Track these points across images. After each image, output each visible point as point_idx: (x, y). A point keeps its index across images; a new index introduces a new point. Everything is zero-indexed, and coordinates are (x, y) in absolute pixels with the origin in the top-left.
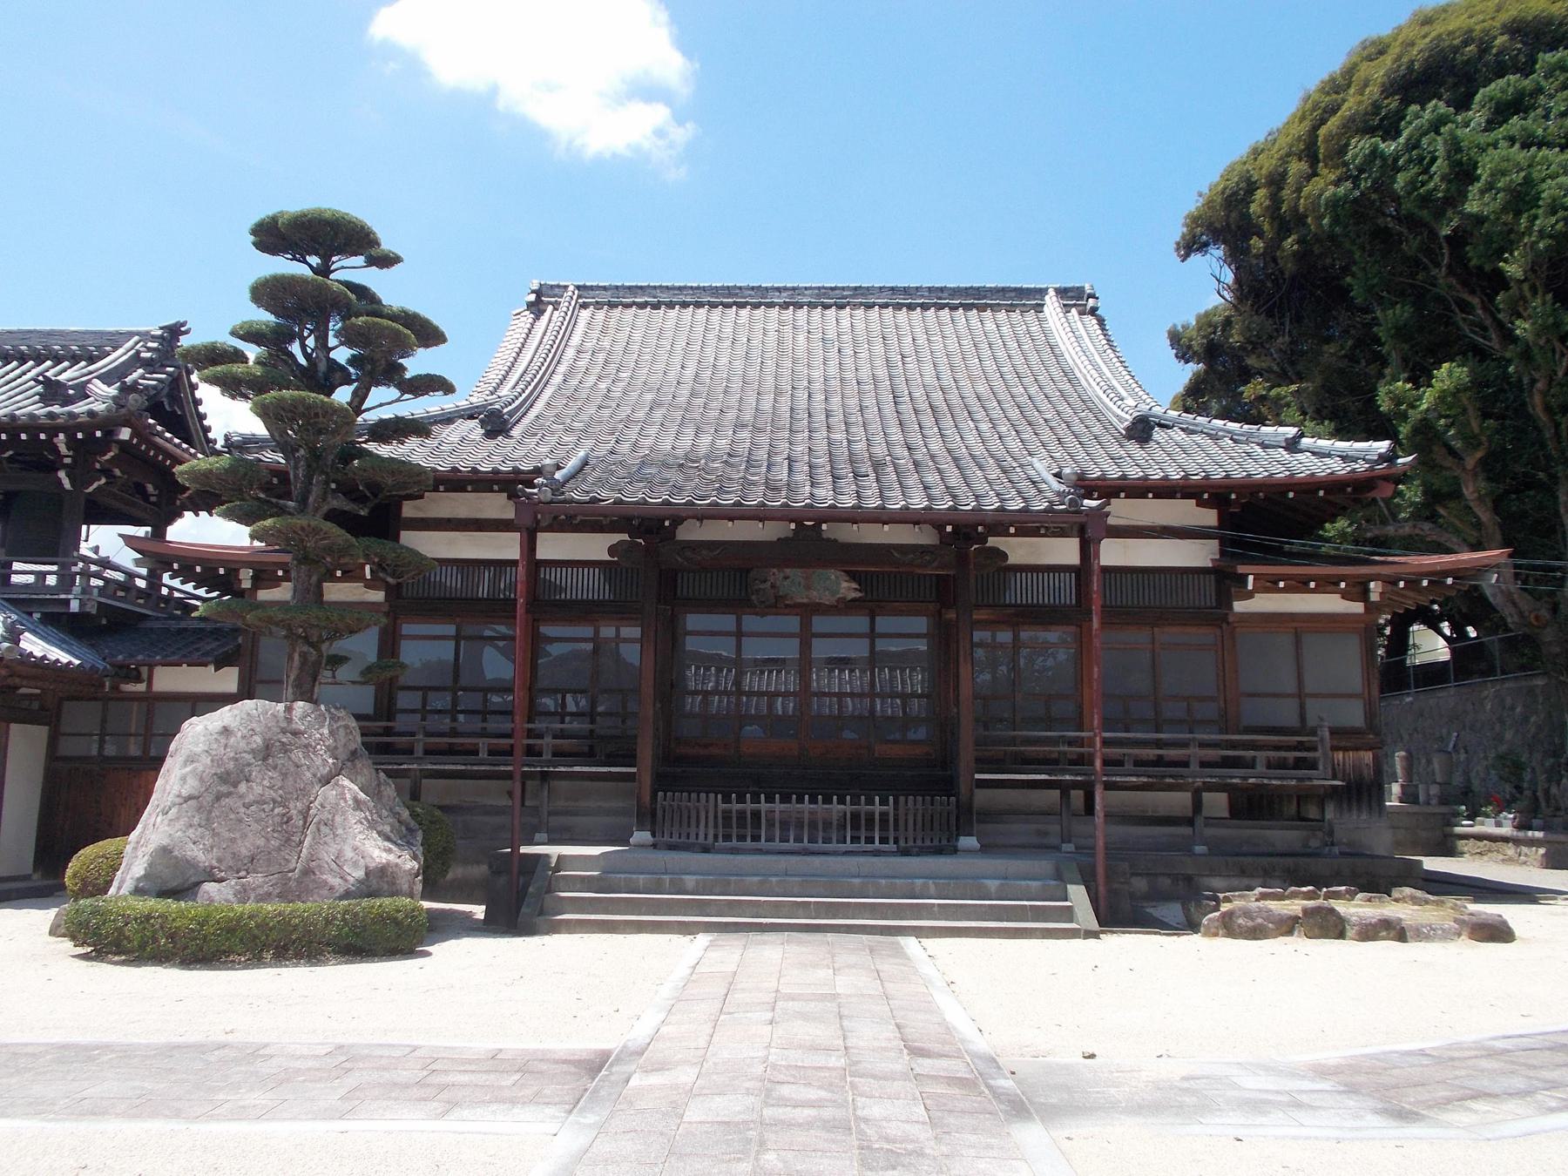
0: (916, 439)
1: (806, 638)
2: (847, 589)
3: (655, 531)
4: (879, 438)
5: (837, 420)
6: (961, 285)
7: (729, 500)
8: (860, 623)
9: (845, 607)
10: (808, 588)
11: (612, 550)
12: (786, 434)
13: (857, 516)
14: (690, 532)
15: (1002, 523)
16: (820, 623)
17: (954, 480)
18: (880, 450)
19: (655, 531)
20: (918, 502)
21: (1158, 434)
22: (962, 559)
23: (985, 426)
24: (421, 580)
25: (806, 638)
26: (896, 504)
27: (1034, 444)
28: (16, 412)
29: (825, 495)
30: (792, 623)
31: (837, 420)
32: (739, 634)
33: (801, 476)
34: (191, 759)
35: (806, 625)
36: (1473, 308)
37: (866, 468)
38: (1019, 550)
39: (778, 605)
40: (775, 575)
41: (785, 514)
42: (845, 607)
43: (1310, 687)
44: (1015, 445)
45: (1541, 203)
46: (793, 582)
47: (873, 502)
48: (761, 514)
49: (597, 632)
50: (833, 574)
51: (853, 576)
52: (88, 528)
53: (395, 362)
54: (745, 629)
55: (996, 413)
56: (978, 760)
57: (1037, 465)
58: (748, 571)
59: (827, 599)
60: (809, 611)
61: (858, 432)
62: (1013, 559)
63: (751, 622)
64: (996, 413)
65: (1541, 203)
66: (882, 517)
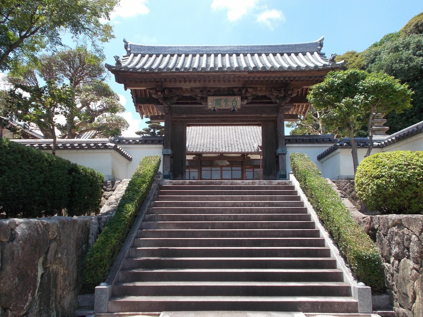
0: (238, 140)
2: (228, 163)
4: (232, 140)
5: (226, 136)
7: (211, 151)
8: (229, 168)
9: (227, 166)
10: (222, 163)
11: (193, 158)
12: (218, 139)
13: (228, 153)
14: (204, 155)
15: (248, 153)
16: (224, 168)
17: (243, 147)
18: (232, 142)
20: (237, 151)
22: (244, 158)
23: (249, 137)
24: (84, 138)
26: (233, 151)
27: (256, 141)
29: (224, 150)
30: (219, 169)
31: (226, 136)
32: (211, 170)
33: (220, 147)
34: (110, 204)
35: (221, 169)
37: (230, 145)
38: (253, 157)
39: (217, 166)
40: (217, 161)
41: (219, 153)
42: (227, 166)
43: (231, 171)
44: (253, 140)
46: (219, 162)
47: (230, 151)
48: (215, 153)
49: (189, 171)
50: (225, 161)
51: (228, 161)
52: (197, 172)
54: (212, 169)
55: (251, 135)
57: (255, 144)
58: (212, 161)
59: (225, 165)
60: (222, 167)
61: (229, 138)
62: (251, 158)
63: (213, 169)
64: (251, 135)
66: (232, 153)
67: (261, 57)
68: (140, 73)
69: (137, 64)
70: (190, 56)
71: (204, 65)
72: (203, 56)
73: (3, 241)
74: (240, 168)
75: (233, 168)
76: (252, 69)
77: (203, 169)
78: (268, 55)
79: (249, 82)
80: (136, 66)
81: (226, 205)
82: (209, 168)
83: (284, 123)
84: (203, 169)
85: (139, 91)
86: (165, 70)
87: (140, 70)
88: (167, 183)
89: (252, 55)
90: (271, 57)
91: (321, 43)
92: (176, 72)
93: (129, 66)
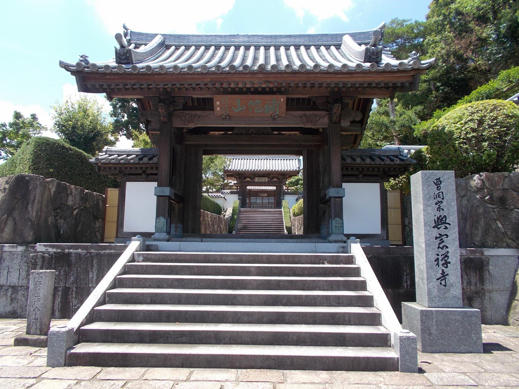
1: (262, 199)
2: (266, 195)
3: (490, 16)
6: (249, 34)
8: (267, 198)
16: (264, 198)
19: (490, 16)
21: (12, 341)
25: (262, 199)
28: (193, 65)
30: (261, 198)
36: (497, 176)
39: (260, 196)
45: (20, 119)
46: (262, 195)
53: (153, 142)
56: (343, 176)
60: (263, 197)
63: (257, 198)
65: (20, 119)
67: (309, 51)
68: (228, 73)
69: (209, 61)
70: (242, 49)
71: (237, 63)
72: (249, 49)
73: (420, 173)
74: (274, 198)
75: (270, 198)
76: (283, 68)
77: (251, 198)
78: (328, 47)
79: (237, 90)
80: (207, 63)
81: (218, 259)
82: (255, 198)
83: (202, 159)
84: (251, 198)
85: (196, 100)
86: (241, 69)
87: (200, 70)
88: (242, 209)
89: (297, 48)
90: (332, 50)
91: (381, 31)
92: (188, 74)
93: (209, 65)
